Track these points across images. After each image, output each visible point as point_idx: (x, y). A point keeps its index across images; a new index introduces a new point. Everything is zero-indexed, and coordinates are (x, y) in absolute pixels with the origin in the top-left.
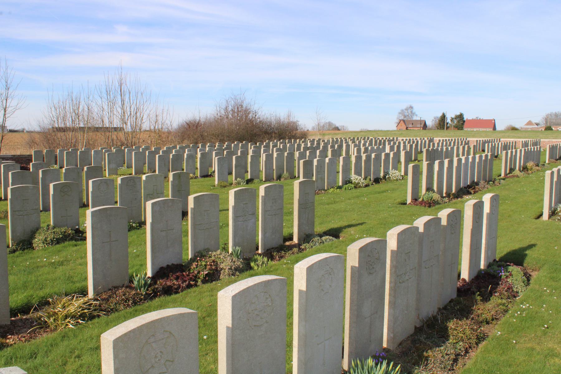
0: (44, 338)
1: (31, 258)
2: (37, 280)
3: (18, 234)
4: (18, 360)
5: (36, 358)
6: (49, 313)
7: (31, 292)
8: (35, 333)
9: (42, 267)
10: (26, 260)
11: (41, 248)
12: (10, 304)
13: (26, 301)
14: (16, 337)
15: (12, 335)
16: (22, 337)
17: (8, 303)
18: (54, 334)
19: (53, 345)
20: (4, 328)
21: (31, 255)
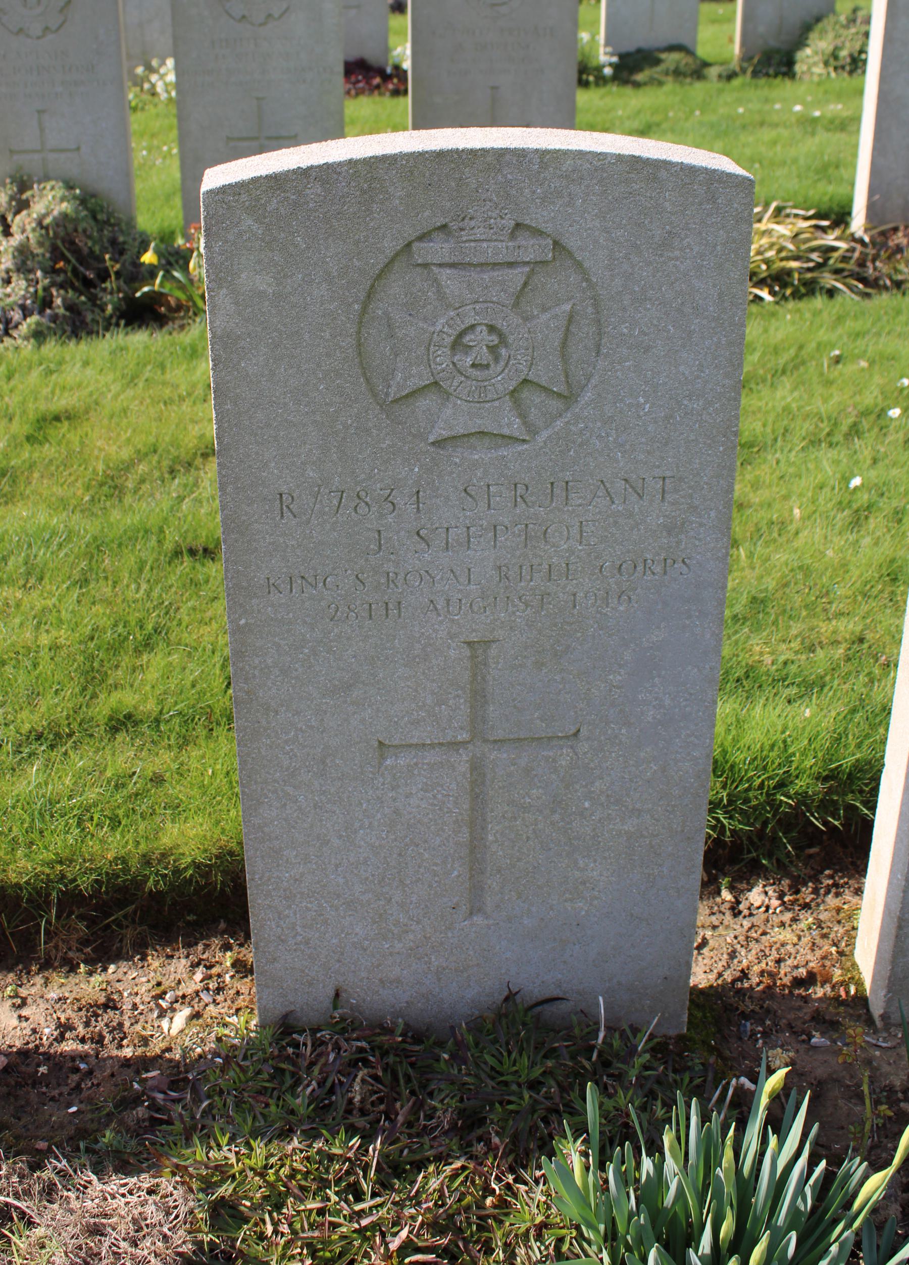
3: (761, 29)
11: (816, 79)
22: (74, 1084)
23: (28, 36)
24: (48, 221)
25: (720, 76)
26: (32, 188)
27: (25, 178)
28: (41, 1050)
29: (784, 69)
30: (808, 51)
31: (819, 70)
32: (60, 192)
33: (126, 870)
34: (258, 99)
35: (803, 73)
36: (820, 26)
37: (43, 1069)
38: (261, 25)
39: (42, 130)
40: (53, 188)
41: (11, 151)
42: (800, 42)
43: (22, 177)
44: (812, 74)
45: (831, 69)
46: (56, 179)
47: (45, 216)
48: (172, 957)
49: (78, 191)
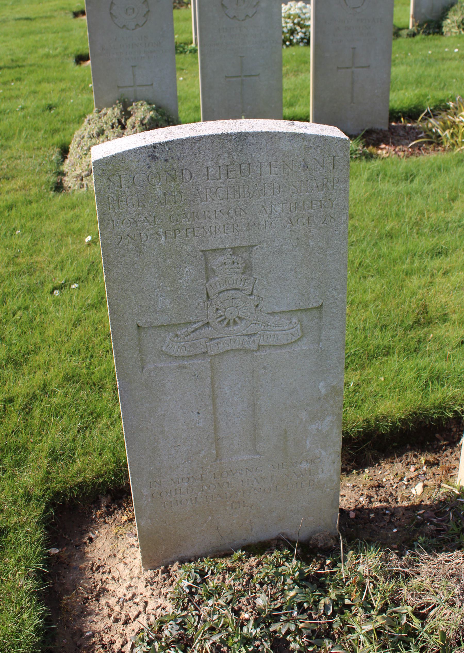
0: (431, 157)
1: (436, 46)
2: (439, 76)
3: (423, 11)
4: (387, 178)
5: (412, 181)
6: (445, 123)
7: (424, 90)
8: (419, 149)
9: (450, 59)
10: (429, 48)
11: (454, 35)
12: (391, 104)
13: (415, 102)
14: (392, 149)
15: (386, 145)
16: (400, 150)
17: (388, 101)
18: (446, 156)
19: (442, 169)
20: (378, 133)
21: (436, 42)
22: (388, 520)
23: (128, 29)
24: (146, 121)
25: (408, 35)
26: (132, 105)
27: (126, 100)
28: (365, 507)
29: (437, 30)
30: (449, 21)
31: (455, 30)
32: (146, 107)
33: (369, 426)
34: (241, 57)
35: (447, 32)
36: (453, 8)
37: (372, 515)
38: (243, 20)
39: (134, 75)
40: (142, 105)
41: (118, 87)
42: (443, 15)
43: (124, 100)
44: (452, 32)
45: (461, 30)
46: (142, 100)
47: (144, 119)
48: (393, 463)
49: (154, 106)
